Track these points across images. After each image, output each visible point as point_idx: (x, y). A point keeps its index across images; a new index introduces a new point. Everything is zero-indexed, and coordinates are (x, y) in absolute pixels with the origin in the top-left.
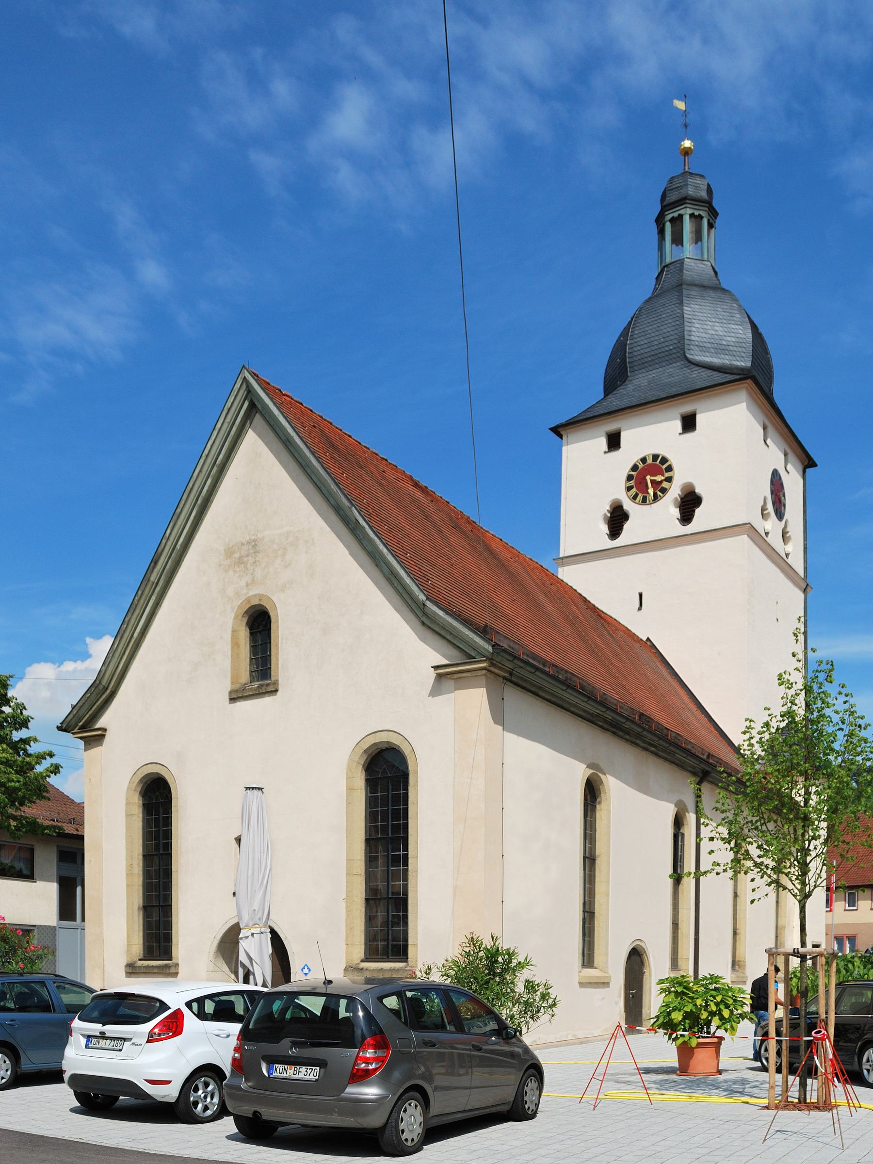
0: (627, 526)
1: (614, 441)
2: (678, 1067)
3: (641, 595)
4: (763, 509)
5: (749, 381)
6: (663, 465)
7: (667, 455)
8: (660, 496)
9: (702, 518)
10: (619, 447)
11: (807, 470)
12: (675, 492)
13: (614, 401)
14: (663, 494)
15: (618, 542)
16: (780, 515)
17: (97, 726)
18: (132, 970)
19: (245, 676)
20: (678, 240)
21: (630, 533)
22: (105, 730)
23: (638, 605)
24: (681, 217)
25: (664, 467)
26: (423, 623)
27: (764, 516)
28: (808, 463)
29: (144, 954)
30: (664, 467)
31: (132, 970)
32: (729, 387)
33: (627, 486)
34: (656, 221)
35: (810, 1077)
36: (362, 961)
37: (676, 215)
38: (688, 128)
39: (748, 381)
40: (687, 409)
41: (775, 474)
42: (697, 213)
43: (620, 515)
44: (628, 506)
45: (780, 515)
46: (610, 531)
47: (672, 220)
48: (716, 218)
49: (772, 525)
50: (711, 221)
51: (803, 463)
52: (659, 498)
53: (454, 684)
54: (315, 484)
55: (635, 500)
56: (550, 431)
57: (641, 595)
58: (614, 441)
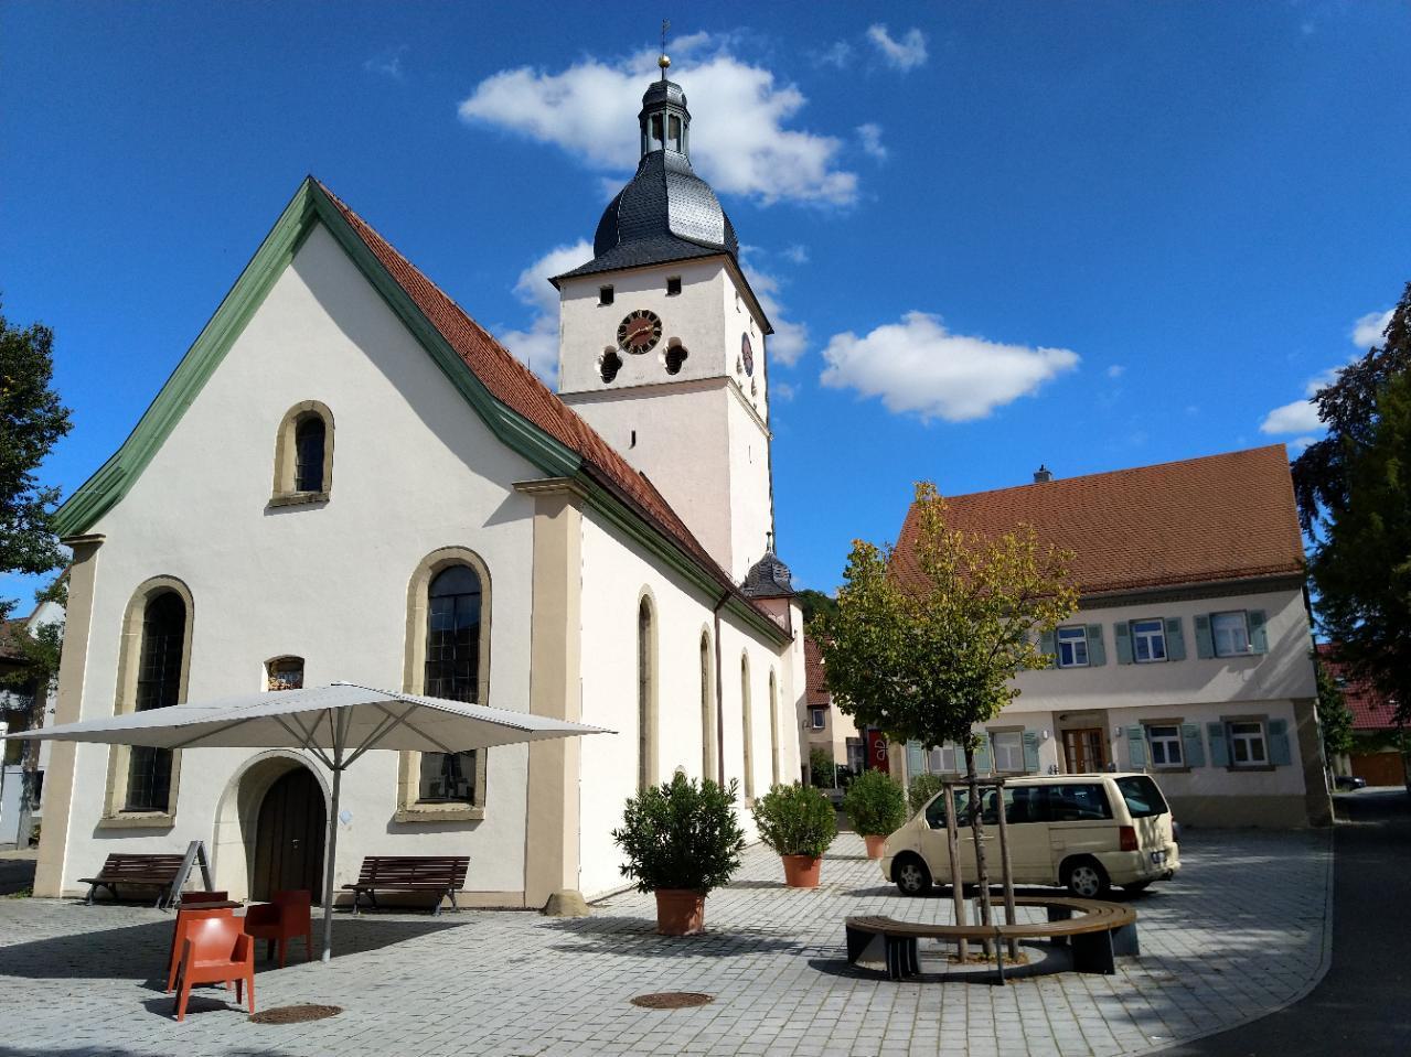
0: (684, 364)
2: (655, 917)
3: (634, 434)
4: (738, 366)
5: (726, 256)
7: (656, 312)
9: (688, 370)
10: (680, 292)
12: (664, 344)
13: (607, 263)
15: (610, 385)
16: (749, 372)
19: (290, 485)
20: (660, 135)
21: (623, 378)
23: (631, 443)
26: (500, 439)
27: (739, 371)
29: (126, 805)
32: (708, 260)
35: (1050, 913)
36: (417, 803)
42: (675, 115)
44: (621, 354)
45: (749, 372)
47: (654, 118)
49: (743, 379)
53: (533, 504)
56: (550, 283)
57: (634, 434)
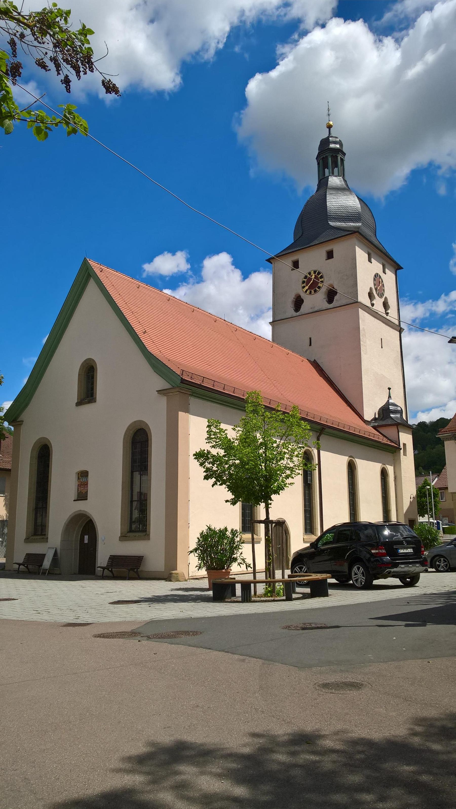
1: (296, 265)
6: (318, 275)
8: (318, 290)
11: (397, 271)
14: (319, 289)
17: (18, 420)
18: (124, 537)
21: (305, 308)
22: (23, 421)
24: (327, 157)
25: (319, 276)
28: (397, 268)
30: (319, 276)
31: (124, 537)
33: (302, 286)
34: (316, 158)
37: (324, 156)
38: (330, 116)
39: (356, 234)
40: (329, 248)
41: (377, 276)
42: (334, 155)
43: (300, 300)
44: (303, 295)
46: (328, 300)
48: (345, 156)
50: (342, 157)
51: (395, 268)
52: (317, 291)
54: (321, 243)
55: (306, 293)
58: (296, 265)
